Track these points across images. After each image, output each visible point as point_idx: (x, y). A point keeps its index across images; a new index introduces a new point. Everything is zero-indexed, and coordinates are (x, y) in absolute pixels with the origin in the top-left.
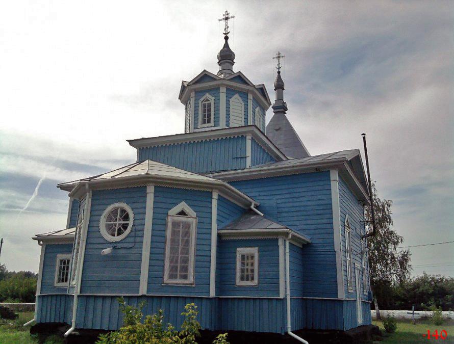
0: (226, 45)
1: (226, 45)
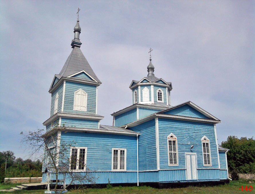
0: (151, 63)
1: (151, 63)
